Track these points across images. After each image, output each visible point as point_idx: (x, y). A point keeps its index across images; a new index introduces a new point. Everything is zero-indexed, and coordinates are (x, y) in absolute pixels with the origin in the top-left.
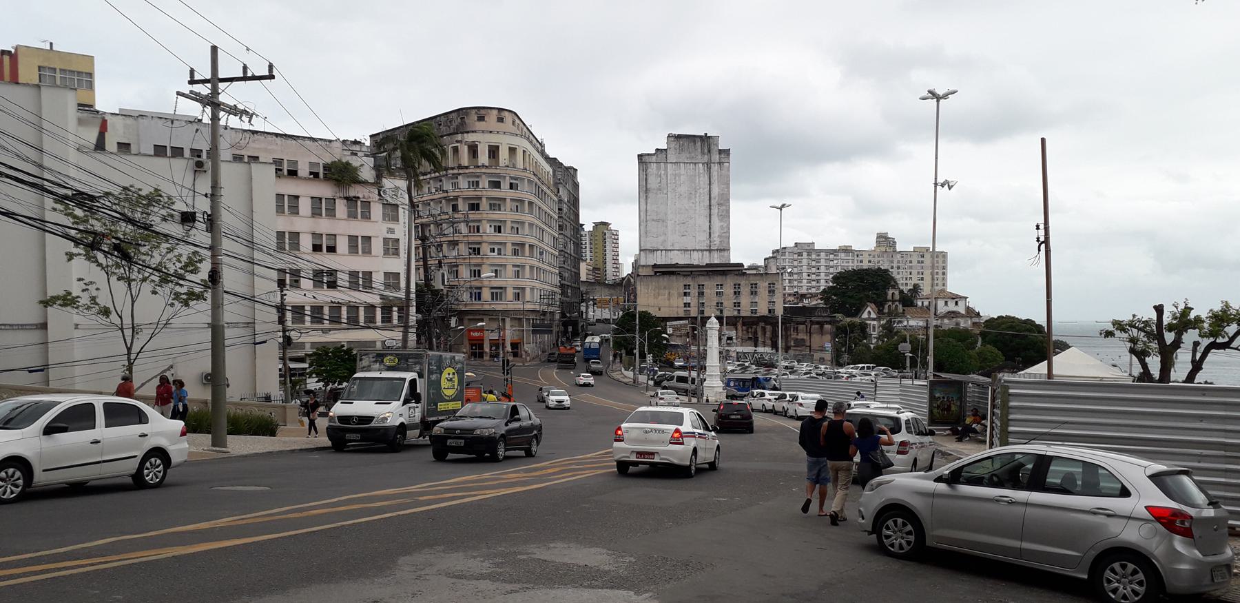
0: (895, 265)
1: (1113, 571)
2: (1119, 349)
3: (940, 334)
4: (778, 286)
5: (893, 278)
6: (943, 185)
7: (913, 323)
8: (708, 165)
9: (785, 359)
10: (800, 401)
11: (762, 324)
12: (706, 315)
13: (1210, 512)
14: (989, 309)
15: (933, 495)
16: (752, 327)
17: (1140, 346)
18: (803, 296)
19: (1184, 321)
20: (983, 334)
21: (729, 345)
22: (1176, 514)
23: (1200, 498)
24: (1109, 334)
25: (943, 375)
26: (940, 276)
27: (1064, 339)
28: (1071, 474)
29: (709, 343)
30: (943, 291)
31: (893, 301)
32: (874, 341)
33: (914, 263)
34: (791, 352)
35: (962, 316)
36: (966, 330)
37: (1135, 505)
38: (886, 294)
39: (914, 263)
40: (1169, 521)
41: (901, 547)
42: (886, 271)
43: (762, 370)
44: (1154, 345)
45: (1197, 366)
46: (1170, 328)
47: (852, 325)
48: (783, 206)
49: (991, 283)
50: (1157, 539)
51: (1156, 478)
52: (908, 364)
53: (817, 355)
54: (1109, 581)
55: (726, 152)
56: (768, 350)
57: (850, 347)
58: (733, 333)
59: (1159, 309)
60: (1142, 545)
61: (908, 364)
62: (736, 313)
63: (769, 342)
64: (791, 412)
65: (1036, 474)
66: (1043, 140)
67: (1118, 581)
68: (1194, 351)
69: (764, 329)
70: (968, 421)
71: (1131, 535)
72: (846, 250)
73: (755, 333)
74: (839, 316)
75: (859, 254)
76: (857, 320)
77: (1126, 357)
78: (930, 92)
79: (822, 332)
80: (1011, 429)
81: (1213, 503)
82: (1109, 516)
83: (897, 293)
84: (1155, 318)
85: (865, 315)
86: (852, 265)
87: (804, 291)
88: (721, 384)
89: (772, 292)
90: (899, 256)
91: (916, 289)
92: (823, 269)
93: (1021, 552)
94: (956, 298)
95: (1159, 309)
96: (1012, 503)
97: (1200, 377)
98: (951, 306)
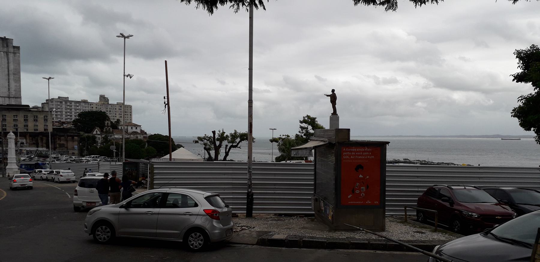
0: (108, 110)
1: (192, 237)
2: (200, 148)
3: (127, 141)
4: (49, 117)
5: (108, 116)
6: (127, 76)
7: (116, 136)
8: (7, 53)
9: (54, 153)
10: (61, 174)
11: (41, 136)
12: (7, 131)
13: (226, 210)
14: (151, 131)
15: (119, 214)
16: (35, 138)
17: (208, 147)
18: (63, 123)
19: (223, 137)
20: (148, 142)
21: (21, 147)
22: (214, 211)
23: (223, 204)
24: (196, 142)
25: (129, 160)
26: (129, 116)
27: (180, 144)
28: (176, 199)
29: (9, 146)
30: (131, 122)
31: (108, 126)
32: (99, 144)
33: (117, 110)
34: (57, 150)
35: (139, 134)
36: (141, 140)
37: (199, 210)
38: (105, 123)
39: (117, 110)
40: (212, 215)
41: (104, 238)
42: (104, 112)
43: (41, 159)
44: (213, 146)
45: (227, 154)
46: (218, 140)
47: (88, 137)
48: (50, 78)
49: (149, 120)
50: (208, 222)
51: (207, 198)
52: (114, 155)
53: (71, 152)
54: (190, 241)
55: (18, 48)
56: (45, 149)
57: (87, 148)
58: (24, 141)
59: (214, 132)
60: (106, 217)
61: (114, 155)
62: (25, 130)
63: (45, 145)
64: (56, 180)
65: (162, 201)
66: (166, 62)
67: (194, 241)
68: (226, 148)
69: (42, 140)
70: (140, 179)
71: (198, 221)
72: (85, 102)
73: (37, 141)
74: (82, 133)
75: (91, 104)
76: (90, 135)
77: (203, 151)
78: (121, 34)
79: (73, 140)
80: (155, 182)
81: (227, 206)
82: (190, 215)
83: (109, 122)
84: (212, 135)
85: (95, 133)
86: (88, 109)
87: (64, 120)
88: (17, 167)
89: (46, 120)
90: (110, 106)
91: (118, 121)
92: (73, 110)
93: (156, 234)
94: (136, 126)
95: (214, 132)
96: (153, 214)
97: (228, 158)
98: (134, 129)
